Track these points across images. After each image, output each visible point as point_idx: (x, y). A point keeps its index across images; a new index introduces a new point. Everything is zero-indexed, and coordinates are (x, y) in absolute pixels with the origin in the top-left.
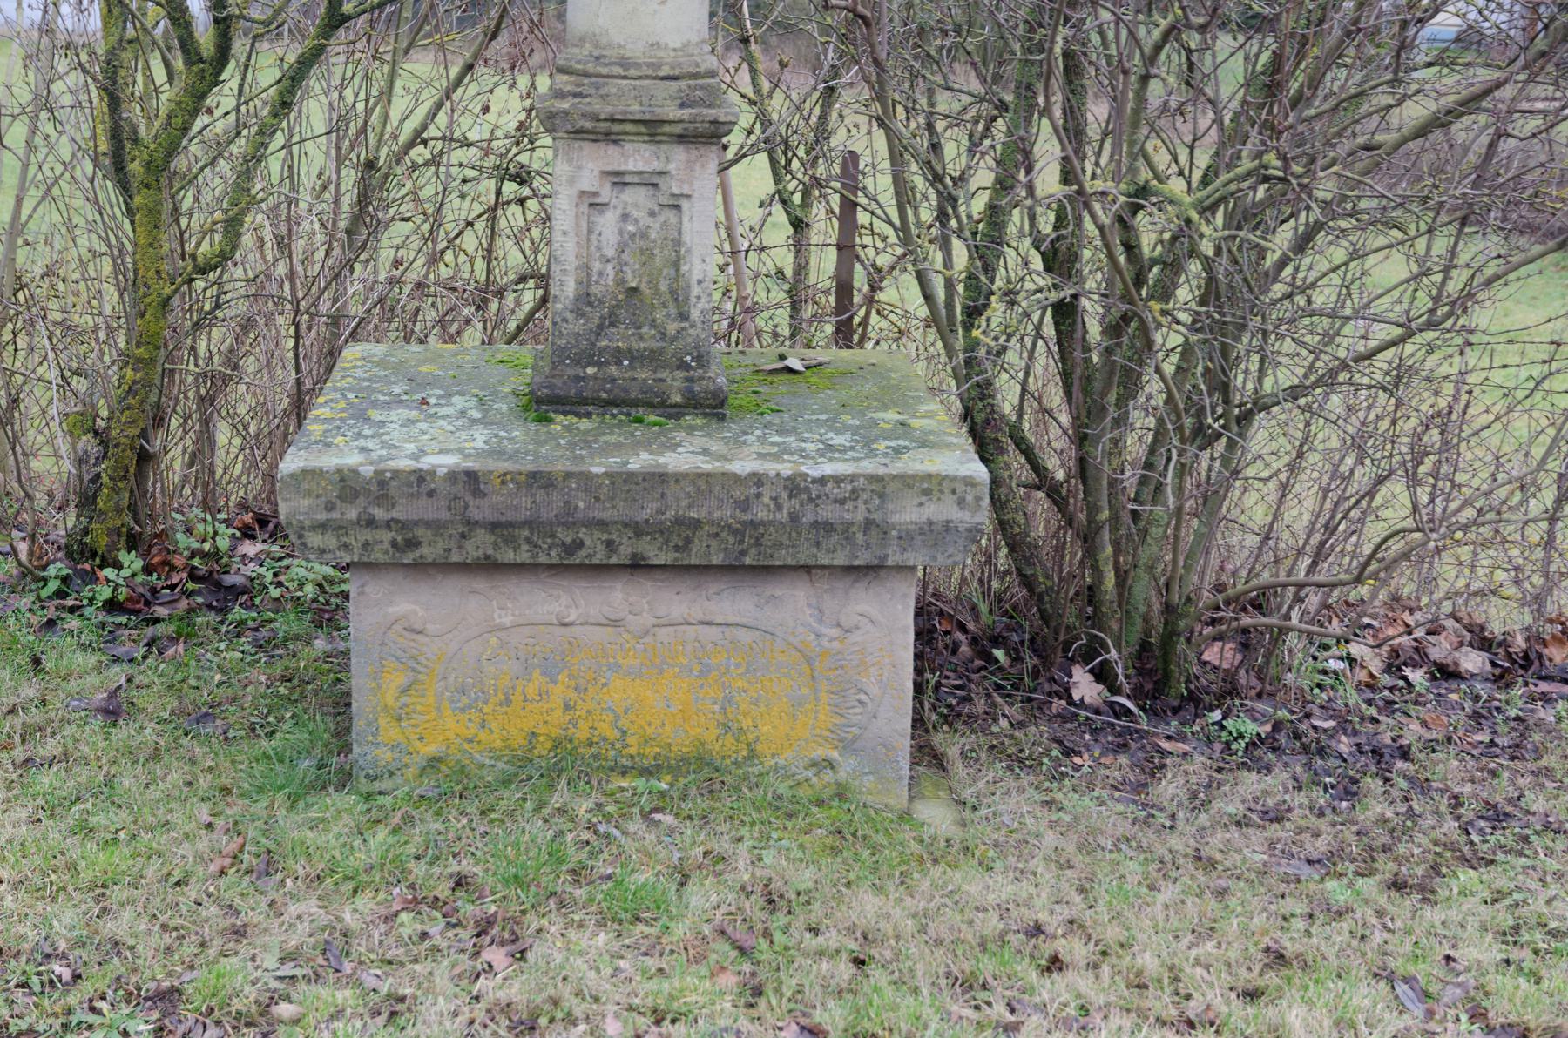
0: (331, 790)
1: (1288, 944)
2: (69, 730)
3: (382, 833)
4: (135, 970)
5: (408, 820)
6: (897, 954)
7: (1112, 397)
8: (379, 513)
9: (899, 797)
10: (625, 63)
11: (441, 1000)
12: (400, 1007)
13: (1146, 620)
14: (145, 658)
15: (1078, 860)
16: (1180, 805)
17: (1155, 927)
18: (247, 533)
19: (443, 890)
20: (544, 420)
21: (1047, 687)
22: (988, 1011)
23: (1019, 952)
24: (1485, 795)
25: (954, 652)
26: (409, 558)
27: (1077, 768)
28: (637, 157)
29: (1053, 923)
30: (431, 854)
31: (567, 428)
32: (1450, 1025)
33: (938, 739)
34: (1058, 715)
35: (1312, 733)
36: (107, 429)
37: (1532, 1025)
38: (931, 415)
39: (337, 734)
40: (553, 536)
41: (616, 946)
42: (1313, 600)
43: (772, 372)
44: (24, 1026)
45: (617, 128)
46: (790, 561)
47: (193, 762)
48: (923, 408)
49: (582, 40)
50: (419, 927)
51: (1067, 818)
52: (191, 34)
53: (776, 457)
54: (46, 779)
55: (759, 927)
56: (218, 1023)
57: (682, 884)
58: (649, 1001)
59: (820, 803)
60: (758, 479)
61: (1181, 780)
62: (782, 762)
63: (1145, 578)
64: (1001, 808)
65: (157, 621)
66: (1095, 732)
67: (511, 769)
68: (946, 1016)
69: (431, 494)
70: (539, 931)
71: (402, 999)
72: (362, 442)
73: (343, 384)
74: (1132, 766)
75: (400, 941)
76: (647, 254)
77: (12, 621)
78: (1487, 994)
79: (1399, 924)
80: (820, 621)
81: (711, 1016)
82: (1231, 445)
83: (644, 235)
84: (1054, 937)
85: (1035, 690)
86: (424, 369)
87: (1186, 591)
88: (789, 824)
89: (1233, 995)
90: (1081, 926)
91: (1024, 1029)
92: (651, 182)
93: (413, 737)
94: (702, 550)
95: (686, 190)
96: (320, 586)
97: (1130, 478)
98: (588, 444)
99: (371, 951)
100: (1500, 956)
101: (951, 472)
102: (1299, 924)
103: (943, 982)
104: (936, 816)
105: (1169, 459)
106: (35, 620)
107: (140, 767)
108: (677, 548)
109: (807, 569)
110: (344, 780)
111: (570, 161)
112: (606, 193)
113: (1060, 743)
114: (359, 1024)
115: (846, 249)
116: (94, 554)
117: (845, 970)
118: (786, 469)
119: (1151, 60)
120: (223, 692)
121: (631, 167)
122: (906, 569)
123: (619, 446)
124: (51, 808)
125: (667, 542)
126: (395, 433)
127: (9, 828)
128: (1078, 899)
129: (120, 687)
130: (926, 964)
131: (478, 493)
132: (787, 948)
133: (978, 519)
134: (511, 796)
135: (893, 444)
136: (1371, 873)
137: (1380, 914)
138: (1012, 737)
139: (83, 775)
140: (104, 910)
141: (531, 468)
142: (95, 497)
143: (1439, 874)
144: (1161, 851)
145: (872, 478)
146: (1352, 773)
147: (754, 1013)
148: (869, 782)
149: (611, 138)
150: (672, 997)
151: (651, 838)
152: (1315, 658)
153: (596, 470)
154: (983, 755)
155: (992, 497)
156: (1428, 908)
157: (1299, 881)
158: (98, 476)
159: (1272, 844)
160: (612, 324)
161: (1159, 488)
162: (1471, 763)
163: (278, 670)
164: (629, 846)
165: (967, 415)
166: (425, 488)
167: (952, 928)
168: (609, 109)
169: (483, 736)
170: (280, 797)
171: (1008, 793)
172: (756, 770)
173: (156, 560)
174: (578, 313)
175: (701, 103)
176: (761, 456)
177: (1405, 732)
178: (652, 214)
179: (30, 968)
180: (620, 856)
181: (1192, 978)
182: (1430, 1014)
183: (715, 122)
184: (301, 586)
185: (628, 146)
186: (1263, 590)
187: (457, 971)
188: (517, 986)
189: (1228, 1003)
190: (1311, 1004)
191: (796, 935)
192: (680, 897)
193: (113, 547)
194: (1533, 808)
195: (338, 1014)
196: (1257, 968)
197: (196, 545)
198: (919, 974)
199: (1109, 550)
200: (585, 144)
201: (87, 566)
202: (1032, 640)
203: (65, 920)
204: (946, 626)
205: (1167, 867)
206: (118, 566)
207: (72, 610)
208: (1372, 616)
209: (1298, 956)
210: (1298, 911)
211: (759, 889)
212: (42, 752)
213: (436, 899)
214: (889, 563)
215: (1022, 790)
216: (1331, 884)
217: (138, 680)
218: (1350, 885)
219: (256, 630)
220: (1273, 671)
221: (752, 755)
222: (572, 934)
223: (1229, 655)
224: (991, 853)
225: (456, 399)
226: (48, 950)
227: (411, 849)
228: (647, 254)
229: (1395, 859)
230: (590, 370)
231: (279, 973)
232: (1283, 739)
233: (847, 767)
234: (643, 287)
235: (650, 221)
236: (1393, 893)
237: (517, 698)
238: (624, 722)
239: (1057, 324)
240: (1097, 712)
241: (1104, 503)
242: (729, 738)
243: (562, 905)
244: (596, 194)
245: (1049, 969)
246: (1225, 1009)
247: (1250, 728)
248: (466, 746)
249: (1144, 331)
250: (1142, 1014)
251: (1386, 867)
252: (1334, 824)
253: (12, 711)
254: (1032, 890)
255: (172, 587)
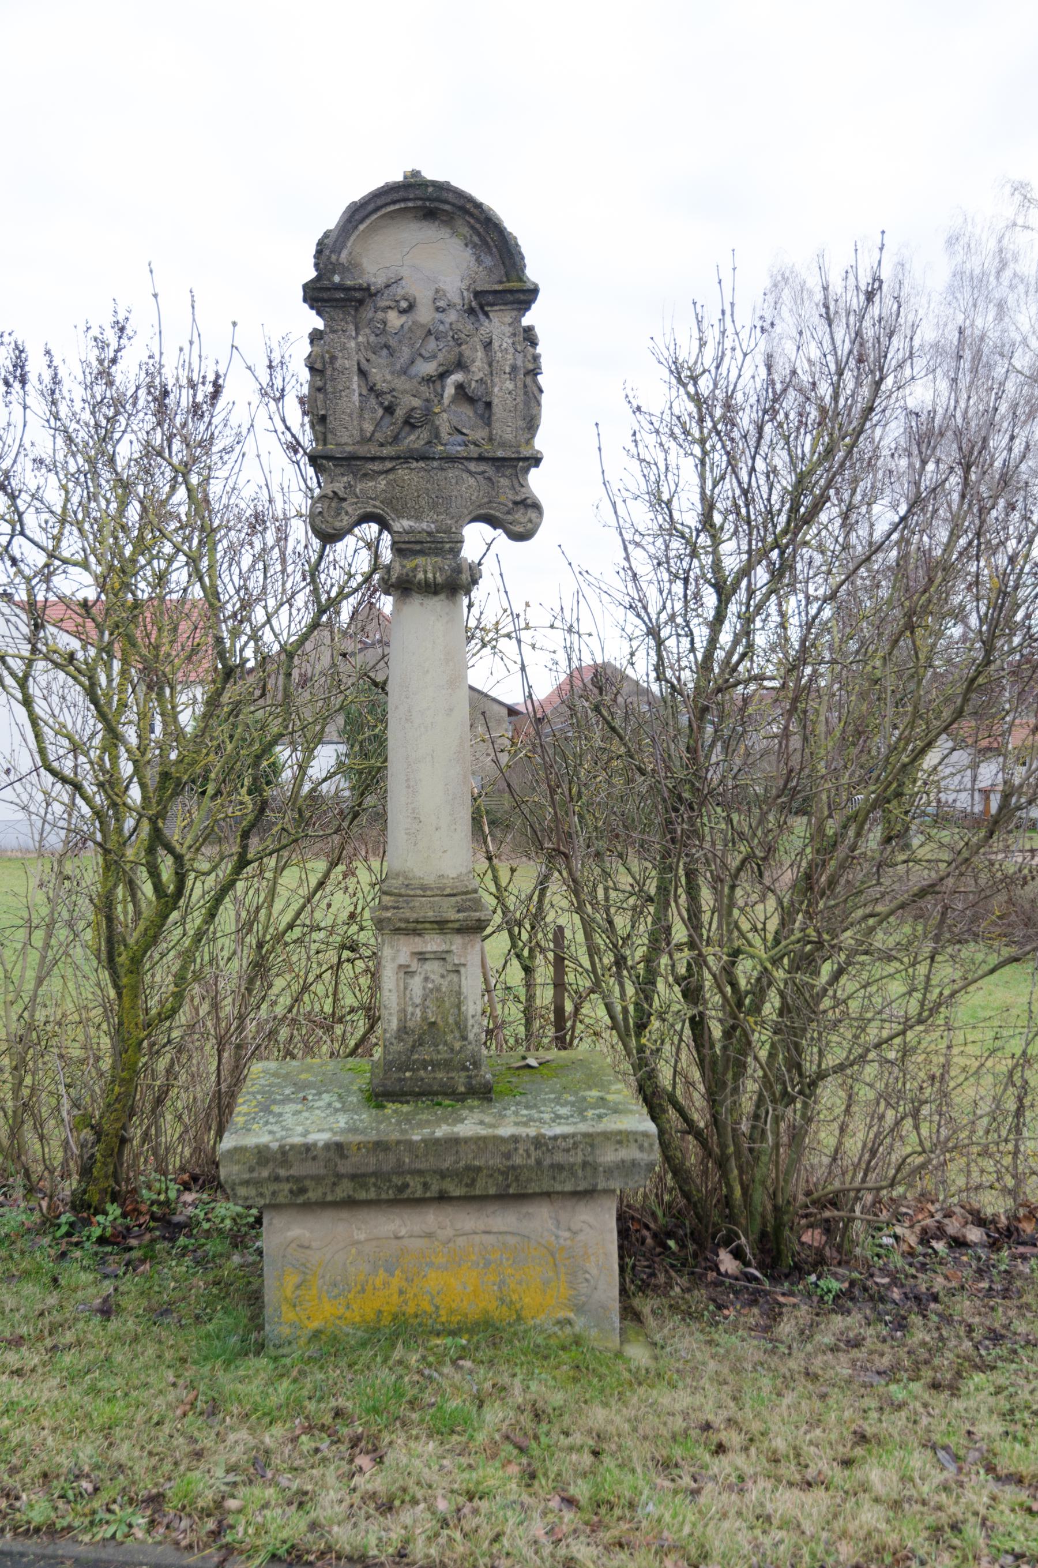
0: (251, 1355)
1: (868, 1428)
2: (81, 1325)
3: (285, 1384)
4: (134, 1483)
5: (302, 1373)
6: (620, 1447)
7: (730, 1075)
8: (282, 1172)
9: (614, 1342)
10: (424, 888)
11: (331, 1492)
12: (305, 1498)
13: (763, 1216)
14: (125, 1274)
15: (731, 1378)
16: (793, 1339)
17: (783, 1420)
18: (187, 1188)
19: (328, 1419)
20: (381, 1107)
21: (703, 1264)
22: (680, 1481)
23: (697, 1441)
24: (988, 1323)
25: (643, 1243)
26: (300, 1200)
27: (726, 1318)
28: (433, 943)
29: (717, 1421)
30: (319, 1395)
31: (395, 1111)
32: (973, 1477)
33: (637, 1302)
34: (712, 1283)
35: (875, 1288)
36: (99, 1124)
37: (1024, 1474)
38: (619, 1092)
39: (252, 1319)
40: (390, 1181)
41: (440, 1450)
42: (869, 1198)
43: (518, 1068)
44: (65, 1523)
45: (420, 926)
46: (537, 1190)
47: (160, 1342)
48: (613, 1088)
49: (398, 875)
50: (313, 1445)
51: (722, 1351)
52: (160, 881)
53: (526, 1124)
54: (67, 1359)
55: (530, 1433)
56: (190, 1515)
57: (480, 1407)
58: (464, 1486)
59: (564, 1348)
60: (515, 1139)
61: (793, 1322)
62: (538, 1322)
63: (760, 1189)
64: (680, 1346)
65: (131, 1249)
66: (736, 1293)
67: (367, 1336)
68: (653, 1487)
69: (314, 1158)
70: (391, 1443)
71: (306, 1493)
72: (269, 1127)
73: (253, 1089)
74: (762, 1315)
75: (302, 1455)
76: (440, 1001)
77: (38, 1253)
78: (995, 1455)
79: (937, 1411)
80: (558, 1227)
81: (505, 1493)
82: (805, 1105)
83: (438, 989)
84: (719, 1430)
85: (696, 1266)
86: (303, 1076)
87: (786, 1196)
88: (545, 1364)
89: (835, 1464)
90: (736, 1423)
91: (704, 1492)
92: (441, 957)
93: (304, 1317)
94: (485, 1186)
95: (463, 961)
96: (234, 1220)
97: (745, 1127)
98: (408, 1121)
99: (283, 1462)
100: (1001, 1430)
101: (634, 1129)
102: (874, 1415)
103: (650, 1464)
104: (638, 1354)
105: (767, 1113)
106: (52, 1252)
107: (127, 1347)
108: (467, 1185)
109: (548, 1195)
110: (260, 1348)
111: (392, 947)
112: (414, 965)
113: (714, 1301)
114: (280, 1511)
115: (559, 985)
116: (89, 1207)
117: (587, 1459)
118: (532, 1132)
119: (736, 876)
120: (178, 1294)
121: (429, 949)
122: (608, 1192)
123: (428, 1121)
124: (73, 1377)
125: (461, 1181)
126: (289, 1120)
127: (46, 1392)
128: (732, 1404)
129: (109, 1295)
130: (639, 1452)
131: (343, 1156)
132: (549, 1446)
133: (652, 1157)
134: (368, 1353)
135: (597, 1112)
136: (918, 1378)
137: (925, 1405)
138: (683, 1298)
139: (91, 1354)
140: (111, 1444)
141: (375, 1138)
142: (91, 1168)
143: (961, 1377)
144: (783, 1370)
145: (586, 1135)
146: (902, 1312)
147: (532, 1490)
148: (594, 1333)
149: (416, 932)
150: (478, 1483)
151: (458, 1377)
152: (873, 1237)
153: (416, 1138)
154: (666, 1312)
155: (661, 1144)
156: (955, 1400)
157: (872, 1386)
158: (93, 1155)
159: (854, 1362)
160: (420, 1045)
161: (763, 1132)
162: (978, 1302)
163: (210, 1278)
164: (445, 1383)
165: (641, 1089)
166: (310, 1155)
167: (653, 1429)
168: (415, 915)
169: (348, 1314)
170: (219, 1362)
171: (683, 1336)
172: (522, 1328)
173: (129, 1208)
174: (400, 1039)
175: (470, 909)
176: (516, 1124)
177: (935, 1284)
178: (443, 976)
179: (67, 1485)
180: (440, 1391)
181: (808, 1453)
182: (960, 1469)
183: (479, 920)
184: (222, 1221)
185: (427, 937)
186: (837, 1193)
187: (340, 1472)
188: (379, 1480)
189: (832, 1469)
190: (884, 1467)
191: (555, 1437)
192: (479, 1415)
193: (102, 1201)
194: (1019, 1331)
195: (265, 1506)
196: (849, 1445)
197: (155, 1197)
198: (635, 1458)
199: (736, 1172)
200: (402, 937)
201: (85, 1215)
202: (692, 1233)
203: (87, 1452)
204: (637, 1226)
205: (788, 1381)
206: (105, 1213)
207: (77, 1244)
208: (908, 1207)
209: (875, 1435)
210: (873, 1406)
211: (529, 1407)
212: (63, 1341)
213: (323, 1425)
214: (599, 1187)
215: (692, 1334)
216: (893, 1387)
217: (122, 1289)
218: (905, 1387)
219: (195, 1251)
220: (846, 1246)
221: (519, 1318)
222: (412, 1444)
223: (817, 1237)
224: (675, 1376)
225: (324, 1096)
226: (77, 1472)
227: (305, 1393)
228: (440, 1001)
229: (933, 1369)
230: (408, 1074)
231: (226, 1480)
232: (856, 1292)
233: (580, 1323)
234: (439, 1021)
235: (441, 981)
236: (932, 1391)
237: (369, 1288)
238: (437, 1300)
239: (692, 1029)
240: (737, 1279)
241: (730, 1142)
242: (505, 1308)
243: (404, 1424)
244: (408, 966)
245: (717, 1452)
246: (830, 1473)
247: (835, 1285)
248: (337, 1322)
249: (745, 1034)
250: (778, 1480)
251: (927, 1374)
252: (893, 1347)
253: (42, 1314)
254: (703, 1400)
255: (140, 1226)
